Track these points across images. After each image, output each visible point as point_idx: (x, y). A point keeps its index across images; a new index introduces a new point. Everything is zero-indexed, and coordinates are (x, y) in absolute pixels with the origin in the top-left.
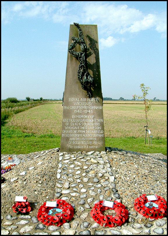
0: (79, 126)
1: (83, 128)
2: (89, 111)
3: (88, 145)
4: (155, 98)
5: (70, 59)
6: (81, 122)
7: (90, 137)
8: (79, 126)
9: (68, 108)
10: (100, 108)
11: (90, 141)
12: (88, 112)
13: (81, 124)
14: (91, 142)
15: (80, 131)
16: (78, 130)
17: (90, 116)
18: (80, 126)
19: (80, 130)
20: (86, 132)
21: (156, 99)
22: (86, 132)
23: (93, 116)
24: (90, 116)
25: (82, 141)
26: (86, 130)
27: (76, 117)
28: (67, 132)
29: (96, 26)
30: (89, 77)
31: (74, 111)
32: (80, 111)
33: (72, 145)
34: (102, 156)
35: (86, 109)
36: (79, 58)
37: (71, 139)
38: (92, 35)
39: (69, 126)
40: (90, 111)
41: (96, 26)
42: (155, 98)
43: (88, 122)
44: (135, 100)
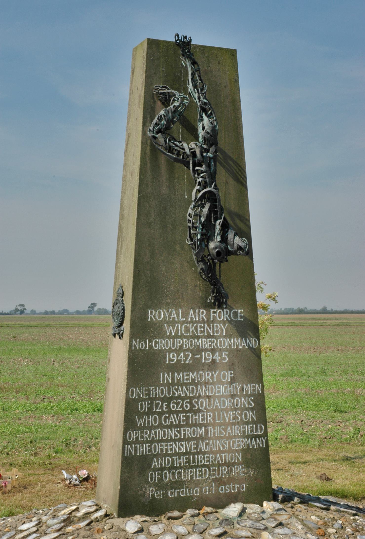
0: (183, 411)
1: (199, 418)
2: (217, 357)
3: (215, 480)
4: (94, 305)
5: (149, 165)
6: (191, 398)
7: (221, 452)
8: (183, 411)
9: (145, 345)
10: (253, 342)
11: (223, 465)
12: (214, 361)
13: (192, 406)
14: (224, 470)
15: (188, 431)
16: (179, 426)
17: (219, 374)
18: (189, 411)
19: (188, 425)
20: (206, 432)
21: (96, 309)
22: (206, 432)
23: (228, 375)
24: (219, 374)
25: (197, 467)
26: (206, 425)
27: (173, 379)
28: (142, 437)
29: (233, 53)
30: (230, 235)
31: (166, 358)
32: (186, 357)
33: (160, 485)
34: (342, 531)
35: (206, 350)
36: (194, 166)
37: (155, 464)
38: (220, 84)
39: (150, 412)
40: (221, 355)
41: (233, 53)
42: (94, 305)
43: (215, 397)
44: (22, 312)
